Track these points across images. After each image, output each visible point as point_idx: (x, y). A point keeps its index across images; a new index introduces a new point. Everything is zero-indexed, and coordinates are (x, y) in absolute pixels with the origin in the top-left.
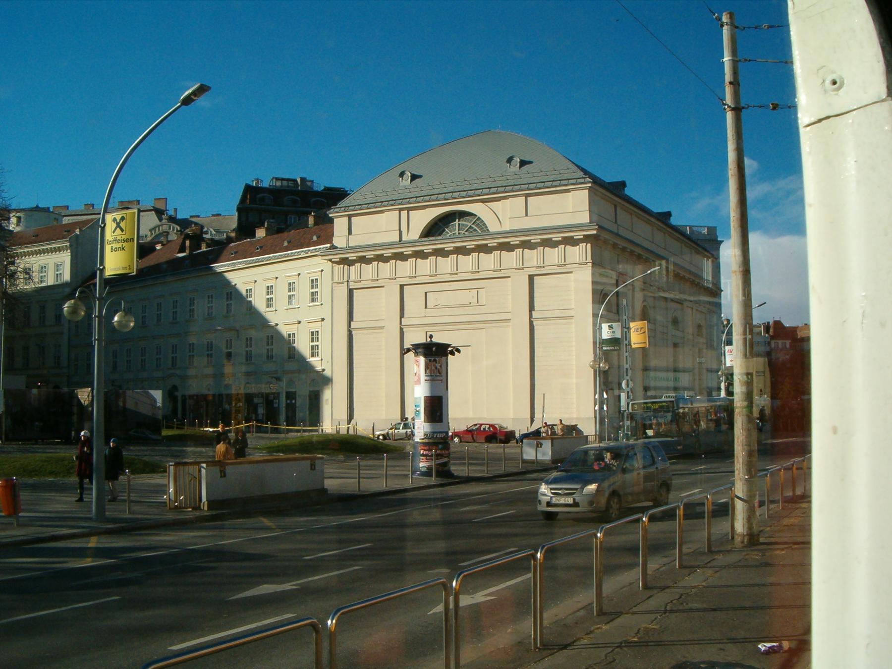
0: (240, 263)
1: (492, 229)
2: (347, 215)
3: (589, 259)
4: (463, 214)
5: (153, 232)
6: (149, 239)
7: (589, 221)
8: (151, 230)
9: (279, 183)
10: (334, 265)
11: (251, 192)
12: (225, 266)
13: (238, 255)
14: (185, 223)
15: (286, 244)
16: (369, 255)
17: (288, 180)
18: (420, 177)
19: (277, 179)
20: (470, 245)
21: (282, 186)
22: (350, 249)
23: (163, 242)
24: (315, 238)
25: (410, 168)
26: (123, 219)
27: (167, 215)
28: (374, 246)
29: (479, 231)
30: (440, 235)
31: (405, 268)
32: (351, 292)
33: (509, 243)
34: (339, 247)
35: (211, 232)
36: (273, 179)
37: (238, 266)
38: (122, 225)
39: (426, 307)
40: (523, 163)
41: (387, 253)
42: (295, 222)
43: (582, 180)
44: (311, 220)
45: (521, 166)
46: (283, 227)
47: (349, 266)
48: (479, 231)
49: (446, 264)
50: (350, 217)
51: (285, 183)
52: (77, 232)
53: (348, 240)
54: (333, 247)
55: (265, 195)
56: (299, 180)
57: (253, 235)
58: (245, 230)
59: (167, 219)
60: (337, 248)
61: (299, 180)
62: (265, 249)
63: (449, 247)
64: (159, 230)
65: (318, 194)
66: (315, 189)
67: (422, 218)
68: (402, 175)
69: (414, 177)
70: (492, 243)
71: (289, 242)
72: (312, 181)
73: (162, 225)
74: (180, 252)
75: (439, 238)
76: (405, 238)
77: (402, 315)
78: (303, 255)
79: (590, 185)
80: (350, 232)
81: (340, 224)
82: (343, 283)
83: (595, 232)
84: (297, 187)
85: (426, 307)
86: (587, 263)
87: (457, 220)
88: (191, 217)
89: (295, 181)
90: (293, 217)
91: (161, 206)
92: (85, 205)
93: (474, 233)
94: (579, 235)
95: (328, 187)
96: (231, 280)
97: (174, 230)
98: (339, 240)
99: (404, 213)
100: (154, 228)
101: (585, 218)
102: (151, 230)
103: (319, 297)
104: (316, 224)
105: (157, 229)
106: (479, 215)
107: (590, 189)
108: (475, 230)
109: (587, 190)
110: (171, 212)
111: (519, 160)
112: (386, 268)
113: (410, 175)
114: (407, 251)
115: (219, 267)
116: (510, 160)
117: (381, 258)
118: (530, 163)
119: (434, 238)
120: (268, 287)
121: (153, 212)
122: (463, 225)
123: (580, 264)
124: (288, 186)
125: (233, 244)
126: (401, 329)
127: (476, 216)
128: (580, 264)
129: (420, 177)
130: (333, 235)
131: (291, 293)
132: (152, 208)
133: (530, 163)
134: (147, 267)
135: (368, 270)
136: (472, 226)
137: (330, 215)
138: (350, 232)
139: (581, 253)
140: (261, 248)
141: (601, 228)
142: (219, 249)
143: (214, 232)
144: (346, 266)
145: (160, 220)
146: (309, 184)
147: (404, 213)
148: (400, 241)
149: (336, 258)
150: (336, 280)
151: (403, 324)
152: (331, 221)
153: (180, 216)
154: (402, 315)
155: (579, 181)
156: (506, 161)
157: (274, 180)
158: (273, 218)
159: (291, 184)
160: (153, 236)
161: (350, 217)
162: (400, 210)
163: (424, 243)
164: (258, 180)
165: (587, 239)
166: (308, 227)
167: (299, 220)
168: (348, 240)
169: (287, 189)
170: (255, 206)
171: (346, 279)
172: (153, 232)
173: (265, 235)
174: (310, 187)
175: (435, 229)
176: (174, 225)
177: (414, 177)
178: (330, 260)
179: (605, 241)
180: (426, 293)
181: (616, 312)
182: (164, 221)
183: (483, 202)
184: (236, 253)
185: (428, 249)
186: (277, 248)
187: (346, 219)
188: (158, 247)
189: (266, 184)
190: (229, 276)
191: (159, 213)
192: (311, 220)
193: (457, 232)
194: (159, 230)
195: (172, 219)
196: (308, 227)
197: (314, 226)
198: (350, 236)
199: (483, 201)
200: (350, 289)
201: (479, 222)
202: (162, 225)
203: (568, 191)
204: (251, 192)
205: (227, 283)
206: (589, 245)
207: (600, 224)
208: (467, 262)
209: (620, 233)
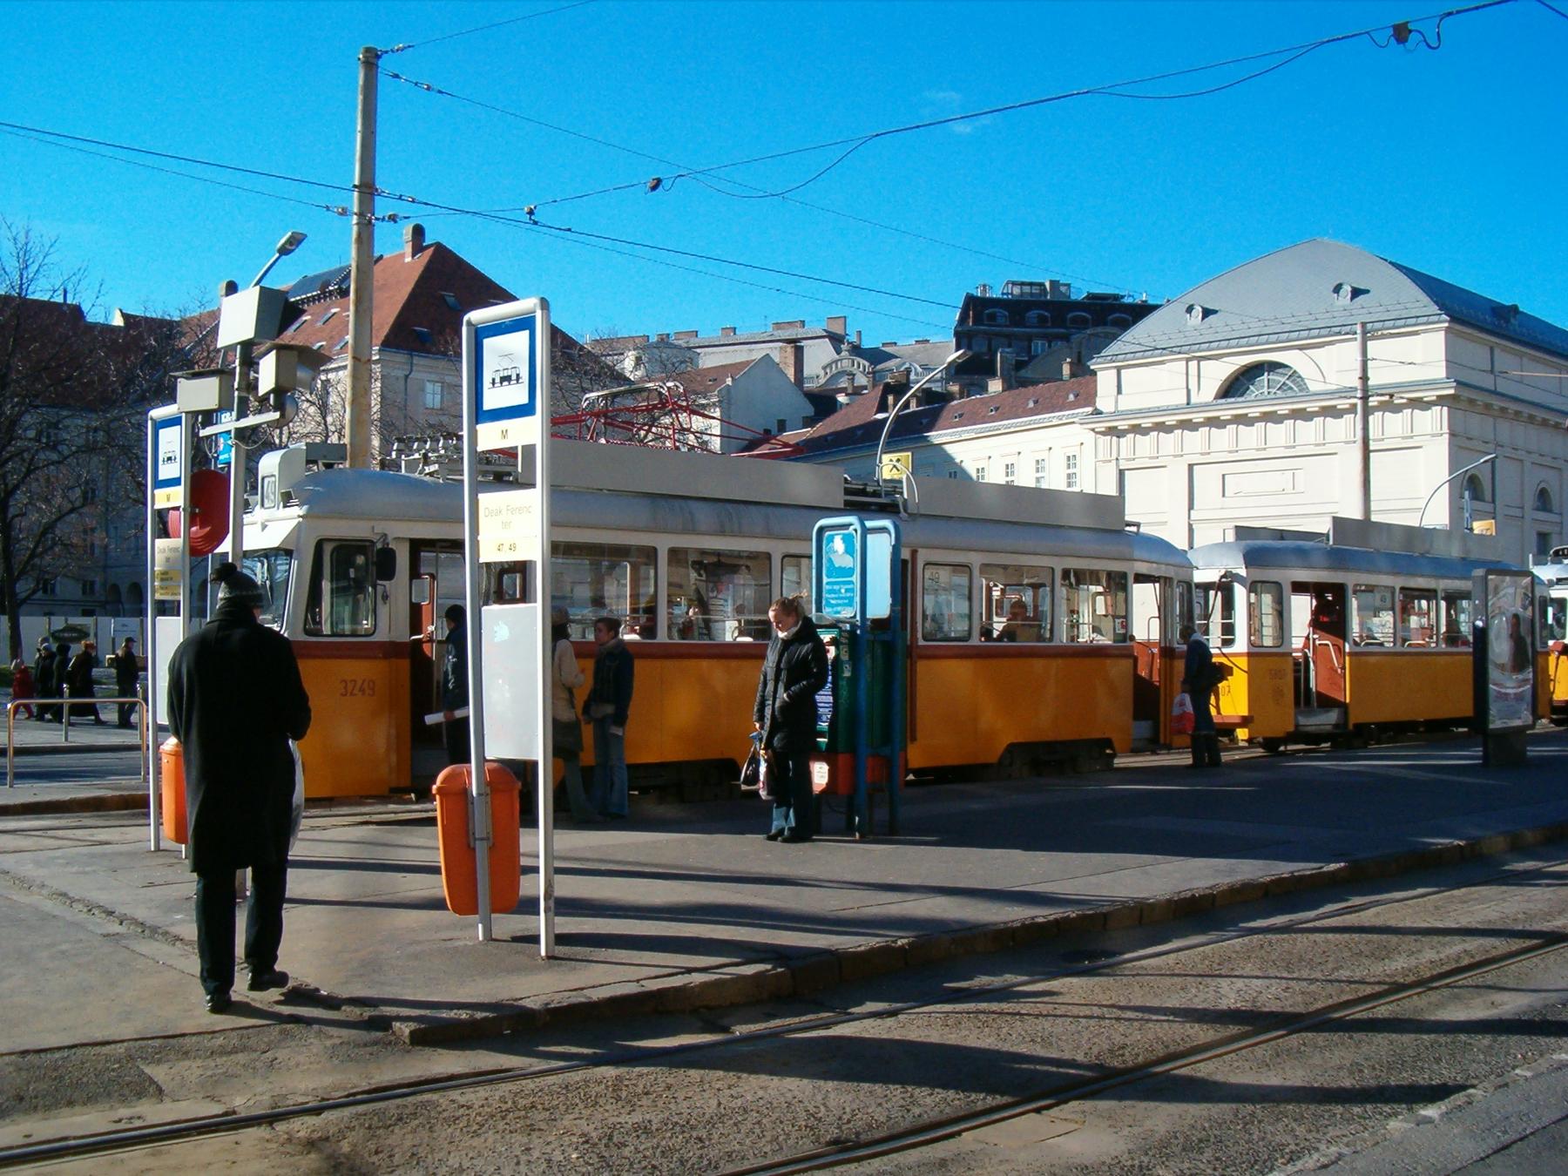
0: (968, 432)
1: (1313, 387)
2: (1115, 367)
3: (1446, 429)
4: (1274, 366)
5: (828, 371)
6: (822, 381)
7: (1444, 375)
8: (824, 368)
9: (1017, 291)
10: (1098, 436)
11: (976, 308)
12: (945, 435)
13: (965, 419)
14: (877, 356)
15: (1031, 405)
16: (1146, 423)
17: (1031, 284)
18: (1214, 312)
19: (1014, 284)
20: (1283, 409)
21: (1022, 294)
22: (1117, 414)
23: (846, 388)
24: (1071, 397)
25: (1203, 298)
26: (898, 460)
27: (849, 343)
28: (1149, 410)
29: (1295, 389)
30: (1242, 395)
31: (1195, 441)
32: (1121, 473)
33: (1335, 407)
34: (1104, 411)
35: (915, 369)
36: (1007, 284)
37: (964, 437)
38: (898, 465)
39: (1224, 496)
40: (1356, 293)
41: (1170, 420)
42: (1043, 350)
43: (1436, 318)
44: (1066, 370)
45: (1352, 298)
46: (1026, 359)
47: (1118, 437)
48: (1295, 389)
49: (1250, 436)
50: (1119, 369)
51: (1027, 289)
52: (729, 381)
53: (1117, 402)
54: (1098, 412)
55: (996, 310)
56: (1048, 285)
57: (984, 389)
58: (971, 371)
59: (848, 351)
60: (1101, 413)
61: (1048, 285)
62: (1001, 411)
63: (1254, 412)
64: (837, 367)
65: (1077, 305)
66: (1073, 297)
67: (1219, 371)
68: (1190, 309)
69: (1207, 313)
70: (1313, 407)
71: (1036, 402)
72: (1068, 285)
73: (841, 360)
74: (877, 412)
75: (1240, 399)
76: (1193, 401)
77: (1191, 507)
78: (1055, 422)
79: (1446, 325)
80: (1119, 391)
81: (1105, 379)
82: (1110, 461)
83: (1452, 391)
84: (1046, 296)
85: (1224, 496)
86: (1442, 435)
87: (1266, 374)
88: (884, 345)
89: (1042, 285)
90: (1040, 342)
91: (838, 330)
92: (723, 329)
93: (1290, 393)
94: (1430, 395)
95: (1093, 294)
96: (954, 455)
97: (859, 367)
98: (1105, 401)
99: (1193, 364)
100: (829, 365)
101: (1440, 372)
102: (824, 368)
103: (1078, 480)
104: (1073, 375)
105: (834, 366)
106: (1295, 368)
107: (1447, 330)
108: (1291, 388)
109: (1443, 332)
110: (853, 338)
111: (1350, 289)
112: (1169, 441)
113: (1200, 309)
114: (1198, 417)
115: (936, 436)
116: (1337, 289)
117: (1161, 427)
118: (1367, 292)
119: (1233, 400)
120: (1007, 466)
121: (827, 340)
122: (1274, 380)
123: (1433, 435)
124: (1032, 294)
125: (955, 402)
126: (1190, 526)
127: (1291, 368)
128: (1433, 435)
129: (1214, 312)
130: (1095, 394)
131: (1039, 475)
132: (825, 334)
133: (1367, 292)
134: (831, 434)
135: (1145, 443)
136: (1287, 382)
137: (1092, 367)
138: (1119, 391)
139: (1435, 421)
140: (997, 409)
141: (1460, 384)
142: (934, 405)
143: (919, 370)
144: (1115, 438)
145: (838, 352)
146: (1063, 289)
147: (1193, 364)
148: (1188, 404)
149: (1101, 427)
150: (1101, 457)
151: (1192, 518)
152: (1094, 373)
153: (867, 344)
154: (1191, 507)
155: (1432, 319)
156: (1332, 289)
157: (1010, 286)
158: (1010, 346)
159: (1035, 290)
160: (828, 376)
161: (1119, 369)
162: (1188, 360)
163: (1219, 407)
164: (984, 286)
165: (1441, 400)
166: (1062, 380)
167: (1050, 346)
168: (1117, 402)
169: (1029, 298)
170: (982, 327)
171: (1114, 456)
172: (828, 371)
173: (1001, 389)
174: (1064, 294)
175: (1234, 387)
176: (859, 359)
177: (1207, 313)
178: (1093, 430)
179: (1471, 401)
180: (1224, 476)
181: (1490, 500)
182: (843, 354)
183: (1300, 349)
184: (961, 416)
185: (1225, 415)
186: (1020, 410)
187: (1114, 372)
188: (842, 398)
189: (996, 293)
190: (949, 449)
191: (836, 340)
192: (1066, 370)
193: (1265, 390)
194: (837, 367)
195: (856, 350)
196: (1062, 380)
197: (1071, 378)
198: (1120, 396)
199: (1301, 348)
200: (1120, 470)
201: (1295, 376)
202: (841, 360)
203: (1416, 333)
204: (976, 308)
205: (949, 459)
206: (1445, 409)
207: (1458, 379)
208: (1279, 433)
209: (1498, 390)
